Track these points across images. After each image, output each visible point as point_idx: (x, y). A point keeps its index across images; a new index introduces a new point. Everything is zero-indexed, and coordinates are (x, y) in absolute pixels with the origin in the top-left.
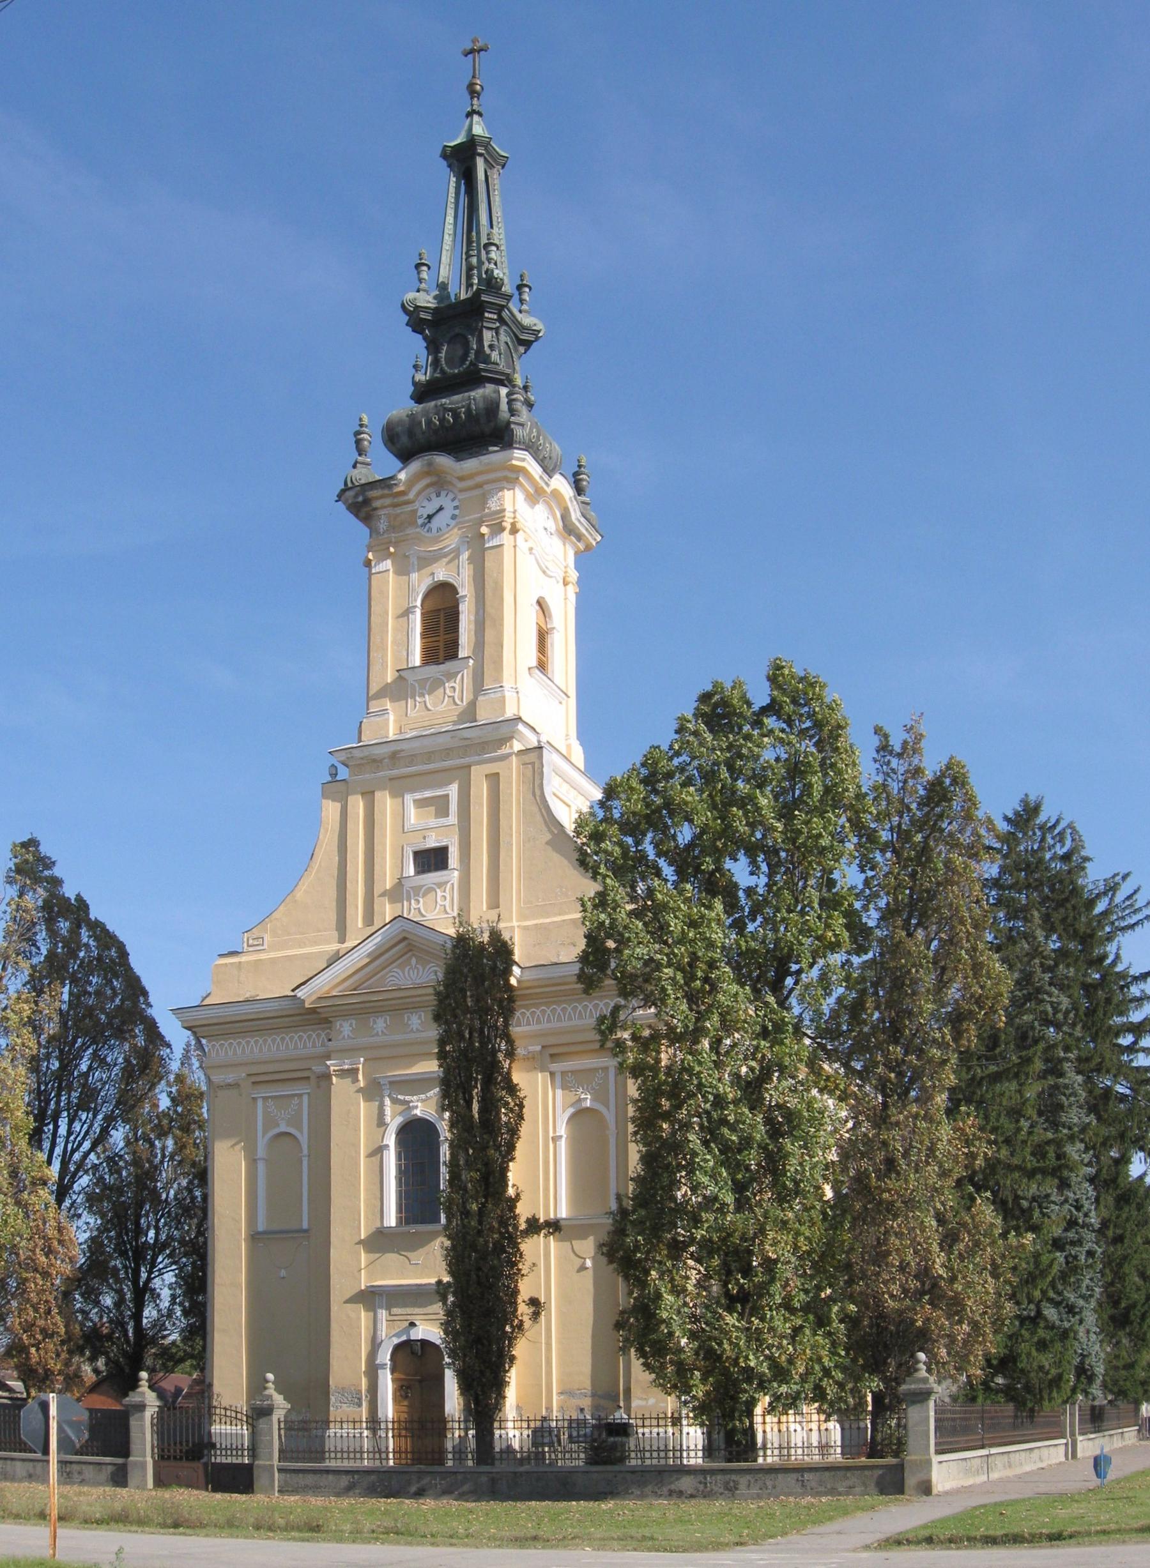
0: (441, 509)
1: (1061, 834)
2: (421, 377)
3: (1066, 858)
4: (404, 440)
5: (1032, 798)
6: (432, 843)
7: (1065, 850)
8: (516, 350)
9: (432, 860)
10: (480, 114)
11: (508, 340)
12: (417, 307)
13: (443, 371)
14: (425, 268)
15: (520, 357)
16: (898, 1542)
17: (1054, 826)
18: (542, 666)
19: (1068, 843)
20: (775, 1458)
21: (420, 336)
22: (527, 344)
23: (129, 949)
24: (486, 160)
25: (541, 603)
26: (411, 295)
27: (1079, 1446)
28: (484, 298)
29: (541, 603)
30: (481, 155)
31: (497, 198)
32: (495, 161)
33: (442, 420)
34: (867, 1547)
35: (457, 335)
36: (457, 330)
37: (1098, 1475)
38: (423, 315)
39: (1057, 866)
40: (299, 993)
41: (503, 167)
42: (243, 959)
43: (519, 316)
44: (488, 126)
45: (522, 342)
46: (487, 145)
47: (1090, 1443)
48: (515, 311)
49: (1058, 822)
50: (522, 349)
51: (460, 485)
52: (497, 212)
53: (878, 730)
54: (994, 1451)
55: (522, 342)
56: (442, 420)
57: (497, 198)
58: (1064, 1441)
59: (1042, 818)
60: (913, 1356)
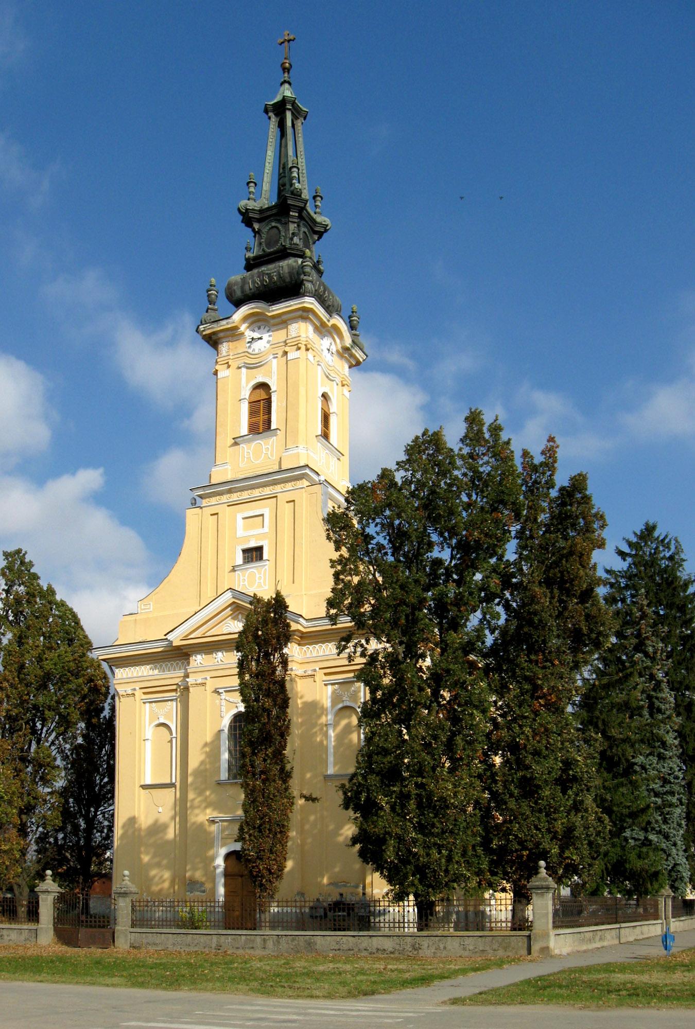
0: (261, 338)
1: (669, 543)
2: (250, 255)
3: (671, 558)
4: (238, 293)
5: (651, 523)
6: (253, 544)
7: (670, 553)
8: (312, 238)
9: (254, 554)
10: (290, 84)
11: (306, 230)
12: (247, 210)
13: (263, 250)
14: (252, 184)
15: (314, 243)
16: (454, 1001)
17: (664, 539)
18: (326, 436)
19: (673, 547)
20: (411, 930)
21: (250, 230)
22: (320, 234)
23: (75, 610)
24: (293, 114)
25: (325, 396)
26: (243, 203)
27: (672, 924)
28: (289, 202)
29: (325, 396)
30: (289, 109)
31: (301, 139)
32: (297, 113)
33: (262, 281)
34: (444, 1003)
35: (273, 227)
36: (273, 224)
37: (666, 949)
38: (251, 215)
39: (664, 564)
40: (169, 637)
41: (305, 119)
42: (138, 617)
43: (315, 216)
44: (295, 91)
45: (315, 232)
46: (293, 103)
47: (681, 923)
48: (312, 214)
49: (666, 536)
50: (316, 237)
51: (272, 321)
52: (301, 148)
53: (497, 417)
54: (623, 925)
55: (315, 232)
56: (262, 281)
57: (301, 139)
58: (660, 921)
59: (656, 534)
60: (537, 863)
